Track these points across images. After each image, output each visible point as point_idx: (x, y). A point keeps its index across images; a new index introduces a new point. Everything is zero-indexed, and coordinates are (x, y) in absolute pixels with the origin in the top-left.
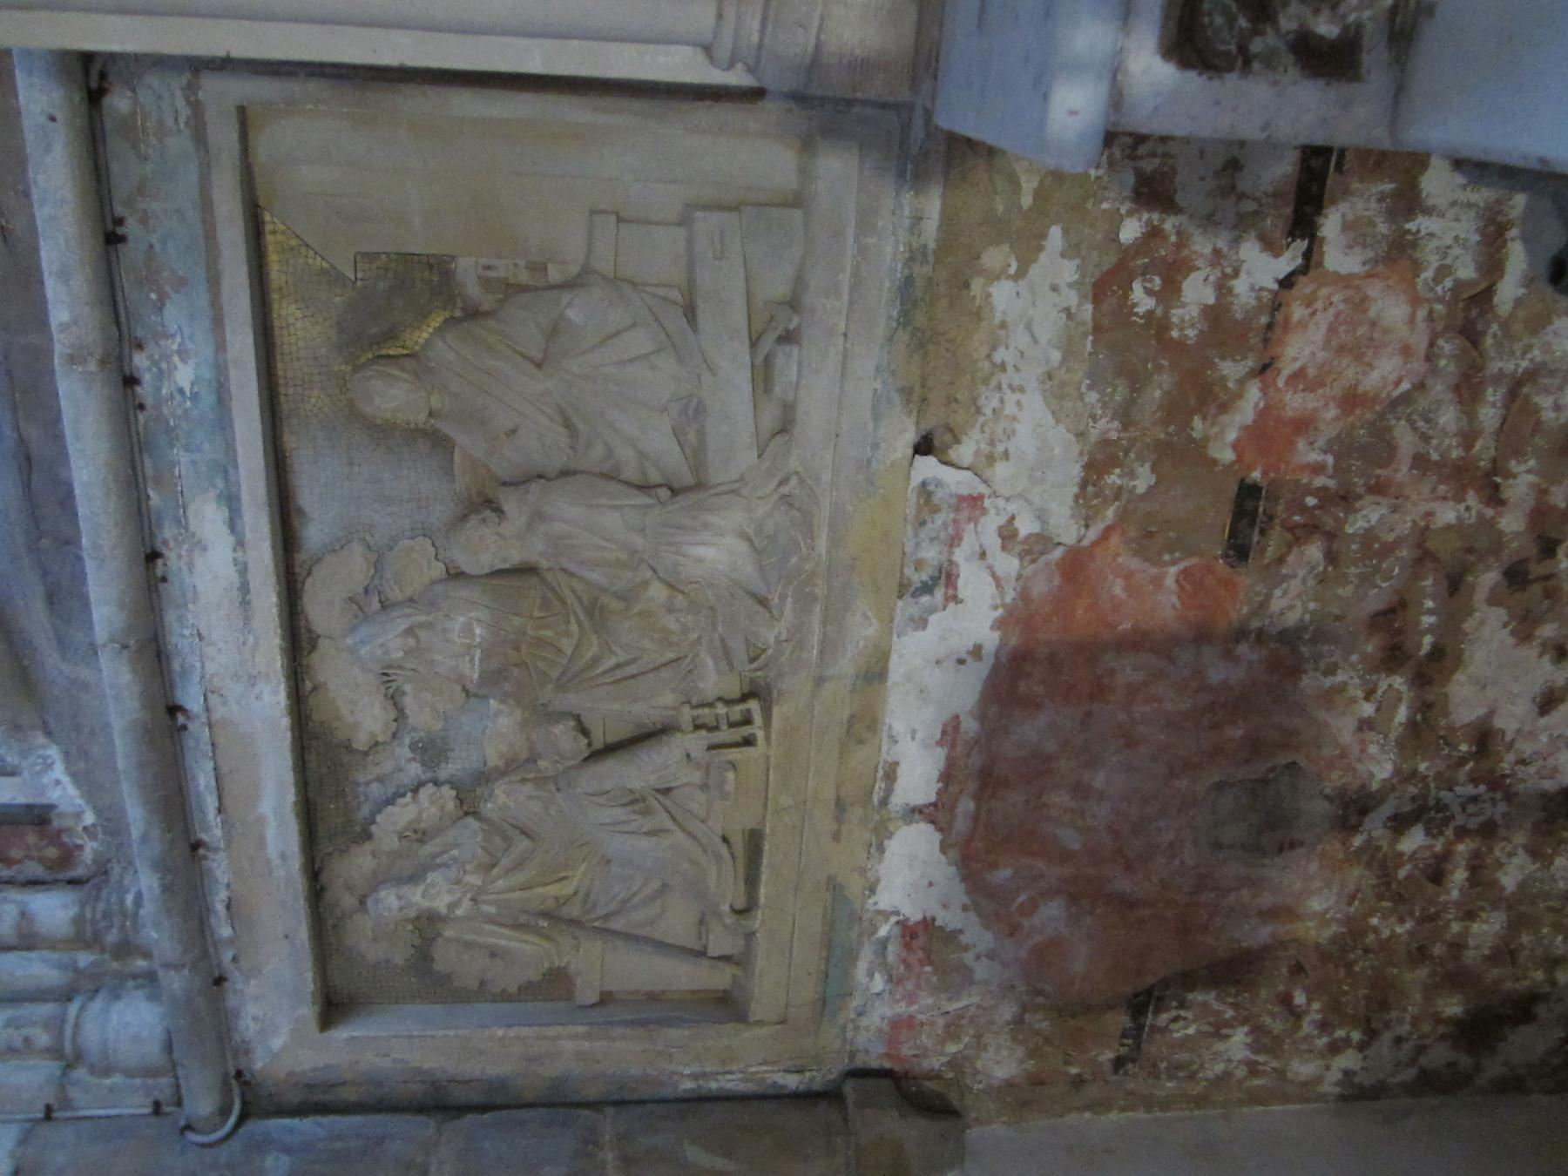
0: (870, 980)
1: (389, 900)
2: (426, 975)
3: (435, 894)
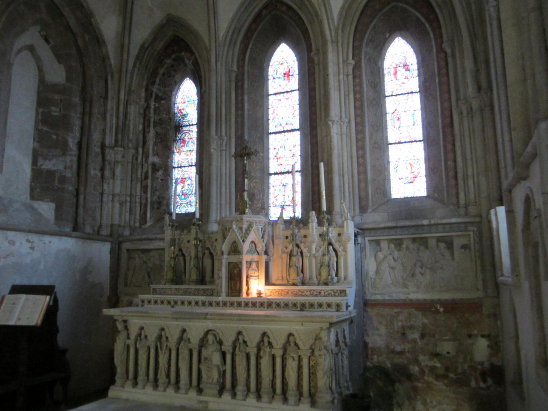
0: (127, 298)
1: (137, 256)
2: (130, 258)
3: (137, 260)
